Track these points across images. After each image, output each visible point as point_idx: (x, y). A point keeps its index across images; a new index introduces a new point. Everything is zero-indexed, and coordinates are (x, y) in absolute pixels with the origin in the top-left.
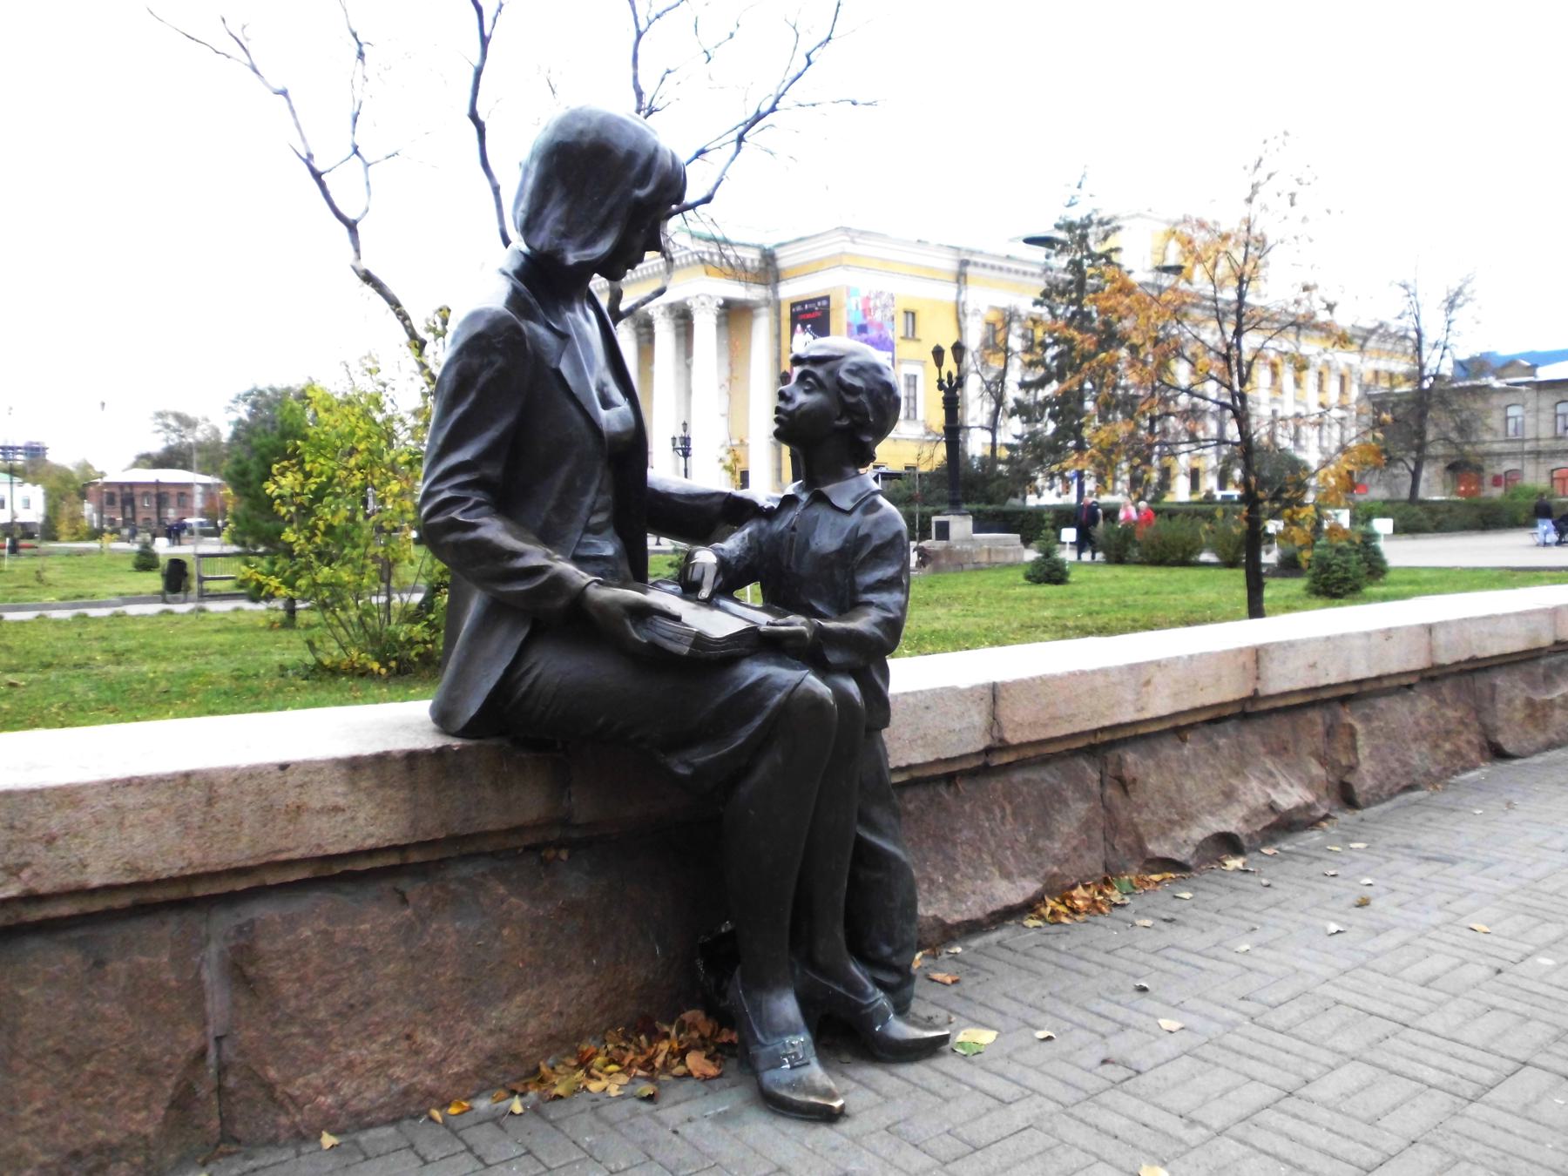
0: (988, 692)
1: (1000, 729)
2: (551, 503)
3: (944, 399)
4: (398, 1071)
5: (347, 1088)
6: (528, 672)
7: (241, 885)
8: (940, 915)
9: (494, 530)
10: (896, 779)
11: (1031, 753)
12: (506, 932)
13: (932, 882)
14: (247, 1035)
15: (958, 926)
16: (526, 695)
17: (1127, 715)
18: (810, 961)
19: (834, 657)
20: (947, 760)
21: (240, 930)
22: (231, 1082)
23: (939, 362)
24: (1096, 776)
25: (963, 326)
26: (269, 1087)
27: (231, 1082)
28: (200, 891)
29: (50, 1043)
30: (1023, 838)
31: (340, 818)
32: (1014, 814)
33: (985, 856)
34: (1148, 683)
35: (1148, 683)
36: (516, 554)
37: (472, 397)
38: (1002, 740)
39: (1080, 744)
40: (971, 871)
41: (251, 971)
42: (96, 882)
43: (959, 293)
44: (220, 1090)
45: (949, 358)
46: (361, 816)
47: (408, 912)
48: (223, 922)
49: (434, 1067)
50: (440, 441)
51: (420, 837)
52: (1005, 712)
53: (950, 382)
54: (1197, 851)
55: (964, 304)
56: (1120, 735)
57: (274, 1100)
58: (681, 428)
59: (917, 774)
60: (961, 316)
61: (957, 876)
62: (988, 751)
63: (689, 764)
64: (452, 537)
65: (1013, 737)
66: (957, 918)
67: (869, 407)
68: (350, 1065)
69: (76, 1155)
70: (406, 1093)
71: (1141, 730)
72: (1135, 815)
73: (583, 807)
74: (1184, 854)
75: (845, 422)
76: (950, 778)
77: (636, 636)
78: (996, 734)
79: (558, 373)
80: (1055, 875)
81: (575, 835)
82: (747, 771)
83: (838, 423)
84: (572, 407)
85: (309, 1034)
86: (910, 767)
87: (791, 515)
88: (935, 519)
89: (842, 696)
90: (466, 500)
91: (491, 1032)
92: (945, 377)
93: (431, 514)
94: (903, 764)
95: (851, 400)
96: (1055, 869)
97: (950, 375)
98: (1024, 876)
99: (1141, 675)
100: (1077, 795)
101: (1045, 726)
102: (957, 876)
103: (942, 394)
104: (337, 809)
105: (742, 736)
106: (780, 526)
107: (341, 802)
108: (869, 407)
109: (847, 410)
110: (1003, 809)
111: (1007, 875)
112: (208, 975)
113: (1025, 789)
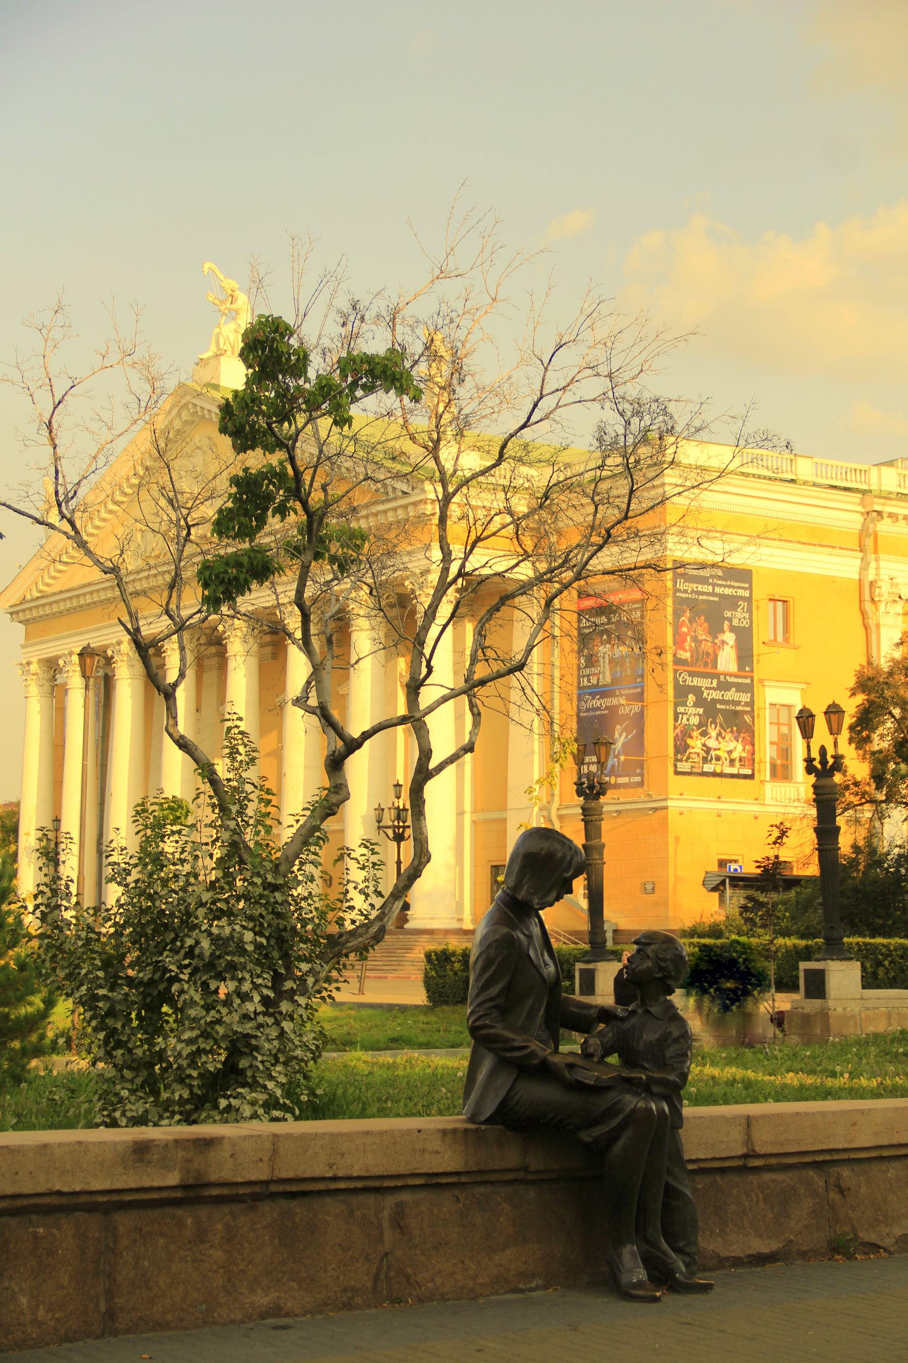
0: (744, 1121)
1: (752, 1144)
2: (524, 1016)
3: (814, 786)
4: (458, 1277)
5: (439, 1281)
6: (516, 1093)
7: (400, 1183)
8: (717, 1250)
9: (499, 1030)
10: (690, 1167)
11: (773, 1161)
12: (502, 1219)
13: (712, 1232)
14: (399, 1253)
15: (727, 1259)
16: (517, 1104)
17: (839, 1143)
18: (646, 1240)
19: (655, 1089)
20: (720, 1159)
21: (397, 1205)
22: (392, 1274)
23: (807, 732)
24: (822, 1183)
25: (872, 623)
26: (408, 1277)
27: (392, 1274)
28: (387, 1183)
29: (337, 1240)
30: (770, 1215)
31: (438, 1156)
32: (765, 1200)
33: (745, 1222)
34: (855, 1124)
35: (855, 1124)
36: (514, 1040)
37: (494, 968)
38: (753, 1150)
39: (808, 1159)
40: (736, 1229)
41: (402, 1223)
42: (355, 1174)
43: (864, 568)
44: (387, 1277)
45: (820, 724)
46: (446, 1156)
47: (461, 1205)
48: (390, 1201)
49: (474, 1278)
50: (480, 984)
51: (468, 1169)
52: (756, 1135)
53: (824, 761)
54: (897, 1242)
55: (872, 584)
56: (836, 1157)
57: (409, 1283)
58: (392, 792)
59: (702, 1165)
60: (868, 606)
61: (728, 1230)
62: (745, 1156)
63: (590, 1136)
64: (484, 1032)
65: (759, 1150)
66: (727, 1254)
67: (671, 968)
68: (440, 1271)
69: (345, 1289)
70: (462, 1287)
71: (853, 1156)
72: (850, 1212)
73: (535, 1162)
74: (888, 1242)
75: (660, 975)
76: (723, 1171)
77: (568, 1076)
78: (749, 1146)
79: (529, 955)
80: (791, 1241)
81: (530, 1177)
82: (615, 1139)
83: (656, 975)
84: (534, 971)
85: (423, 1254)
86: (698, 1160)
87: (634, 1020)
88: (803, 965)
89: (661, 1112)
90: (491, 1014)
91: (496, 1266)
92: (815, 754)
93: (474, 1021)
94: (694, 1157)
95: (663, 964)
96: (792, 1237)
97: (823, 751)
98: (770, 1238)
99: (853, 1120)
100: (807, 1193)
101: (781, 1144)
102: (728, 1230)
103: (812, 779)
104: (438, 1152)
105: (615, 1122)
106: (627, 1026)
107: (439, 1148)
108: (671, 968)
109: (661, 969)
110: (757, 1196)
111: (760, 1236)
112: (386, 1224)
113: (772, 1185)
